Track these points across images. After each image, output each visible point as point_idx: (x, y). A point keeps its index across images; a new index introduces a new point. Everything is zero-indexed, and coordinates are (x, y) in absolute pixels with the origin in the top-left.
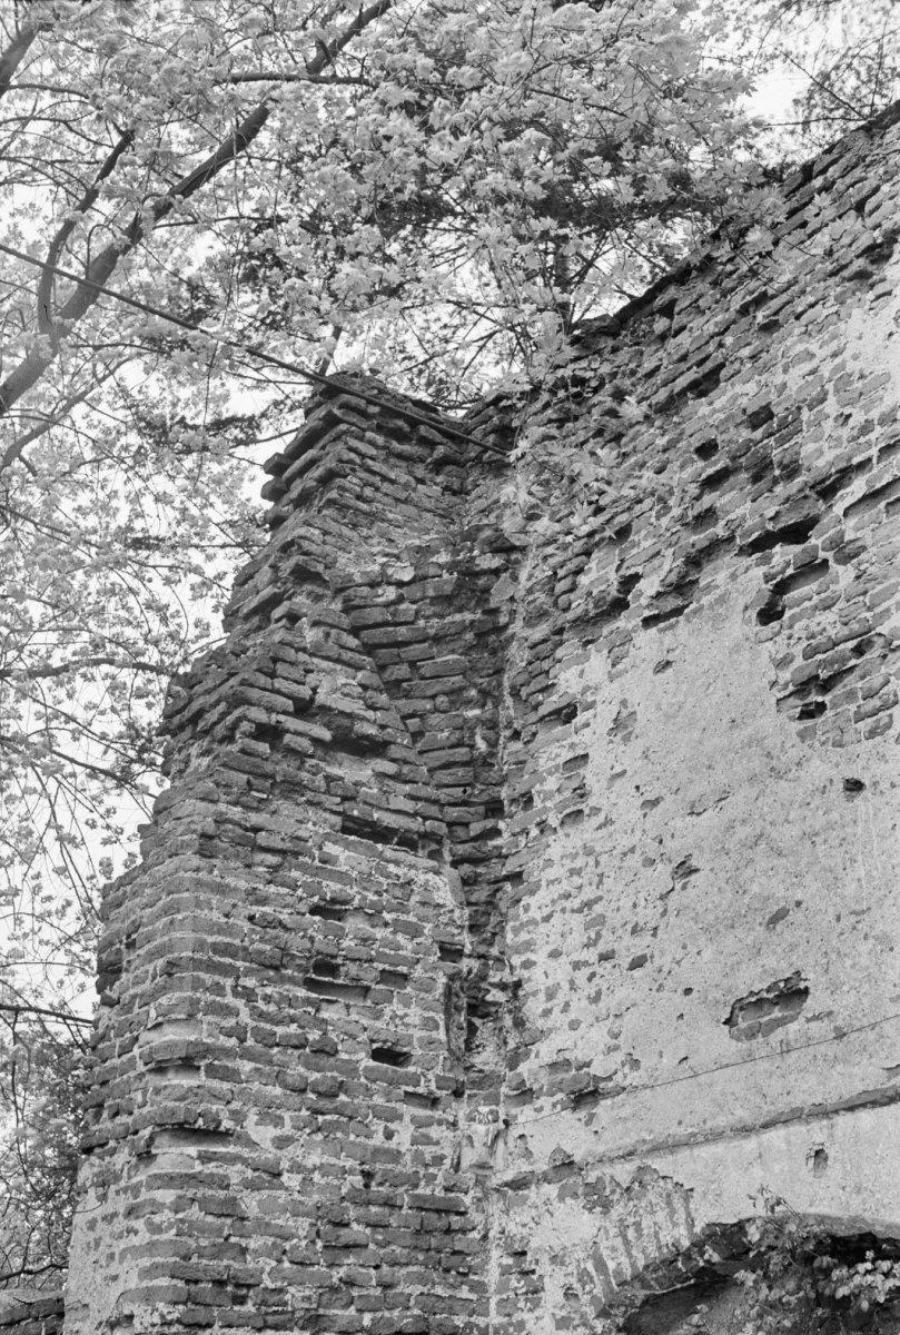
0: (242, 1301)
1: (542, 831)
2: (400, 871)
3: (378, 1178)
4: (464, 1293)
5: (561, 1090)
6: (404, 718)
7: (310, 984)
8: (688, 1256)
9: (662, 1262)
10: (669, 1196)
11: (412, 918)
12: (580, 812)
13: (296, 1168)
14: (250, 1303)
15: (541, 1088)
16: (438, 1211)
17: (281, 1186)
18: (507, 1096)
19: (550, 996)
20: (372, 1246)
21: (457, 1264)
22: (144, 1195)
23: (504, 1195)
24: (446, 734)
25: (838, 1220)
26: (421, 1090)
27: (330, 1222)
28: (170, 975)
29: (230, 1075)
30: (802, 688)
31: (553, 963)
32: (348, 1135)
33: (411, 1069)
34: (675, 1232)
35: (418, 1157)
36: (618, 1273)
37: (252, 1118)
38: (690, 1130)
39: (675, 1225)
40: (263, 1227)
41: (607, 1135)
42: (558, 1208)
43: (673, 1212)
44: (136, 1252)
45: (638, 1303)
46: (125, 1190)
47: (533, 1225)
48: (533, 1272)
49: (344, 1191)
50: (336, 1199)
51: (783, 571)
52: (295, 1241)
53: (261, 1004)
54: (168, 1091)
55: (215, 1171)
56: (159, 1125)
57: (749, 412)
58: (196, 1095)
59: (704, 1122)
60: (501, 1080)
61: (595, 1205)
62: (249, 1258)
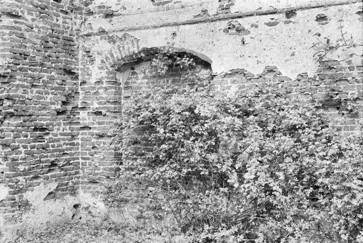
0: (25, 59)
3: (55, 31)
4: (74, 60)
5: (102, 13)
8: (136, 55)
9: (130, 56)
10: (133, 41)
13: (37, 27)
15: (96, 12)
17: (33, 31)
18: (84, 13)
20: (54, 48)
21: (71, 53)
23: (84, 38)
26: (64, 9)
27: (45, 41)
32: (48, 19)
33: (62, 4)
34: (134, 49)
35: (64, 27)
36: (117, 57)
37: (26, 13)
38: (140, 26)
40: (30, 41)
41: (115, 25)
42: (100, 41)
43: (133, 45)
47: (92, 45)
48: (92, 56)
49: (48, 34)
50: (46, 36)
52: (37, 45)
54: (5, 3)
55: (18, 26)
56: (3, 12)
58: (13, 5)
59: (144, 24)
60: (83, 9)
62: (27, 48)
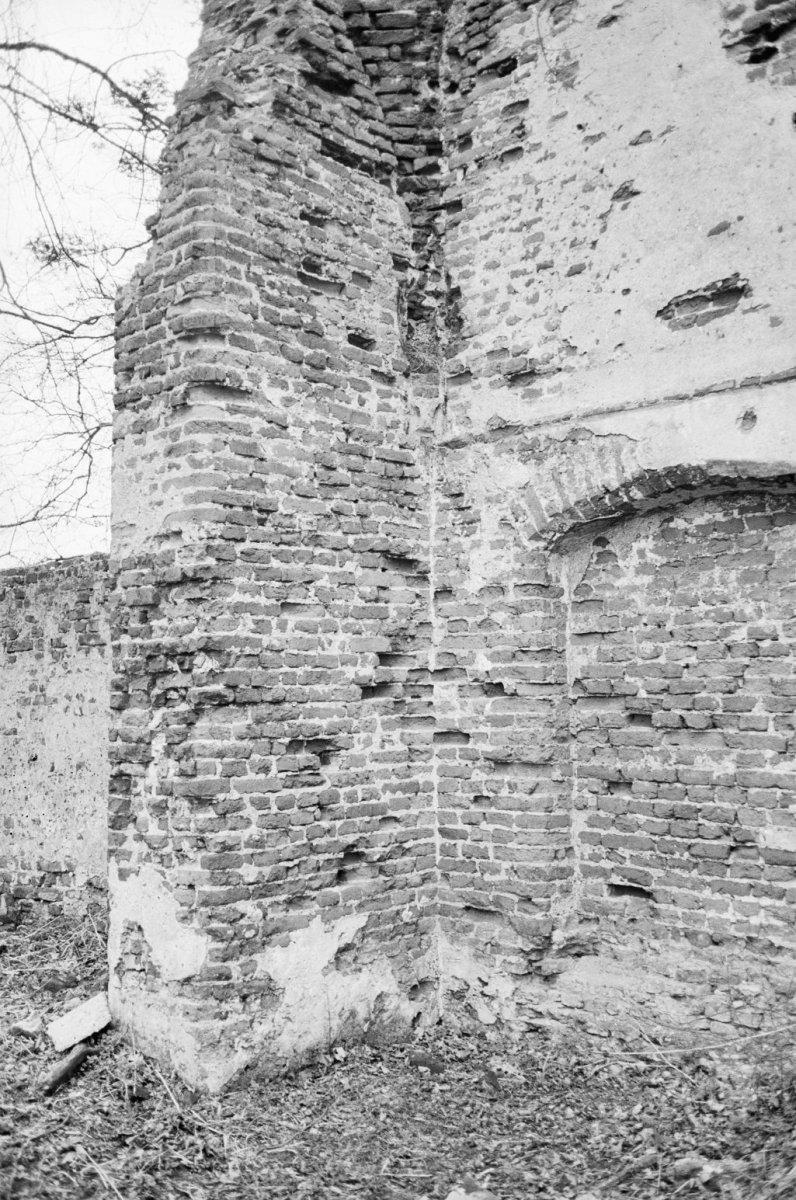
0: (262, 522)
1: (480, 167)
2: (366, 192)
4: (413, 523)
6: (366, 62)
7: (301, 276)
8: (615, 493)
11: (371, 231)
13: (299, 423)
14: (268, 524)
16: (395, 462)
19: (488, 298)
22: (183, 439)
24: (398, 80)
26: (383, 369)
28: (196, 257)
29: (245, 344)
31: (490, 274)
34: (606, 476)
36: (549, 508)
39: (606, 471)
40: (278, 468)
44: (181, 482)
45: (566, 529)
46: (163, 435)
53: (267, 289)
55: (240, 421)
62: (268, 491)
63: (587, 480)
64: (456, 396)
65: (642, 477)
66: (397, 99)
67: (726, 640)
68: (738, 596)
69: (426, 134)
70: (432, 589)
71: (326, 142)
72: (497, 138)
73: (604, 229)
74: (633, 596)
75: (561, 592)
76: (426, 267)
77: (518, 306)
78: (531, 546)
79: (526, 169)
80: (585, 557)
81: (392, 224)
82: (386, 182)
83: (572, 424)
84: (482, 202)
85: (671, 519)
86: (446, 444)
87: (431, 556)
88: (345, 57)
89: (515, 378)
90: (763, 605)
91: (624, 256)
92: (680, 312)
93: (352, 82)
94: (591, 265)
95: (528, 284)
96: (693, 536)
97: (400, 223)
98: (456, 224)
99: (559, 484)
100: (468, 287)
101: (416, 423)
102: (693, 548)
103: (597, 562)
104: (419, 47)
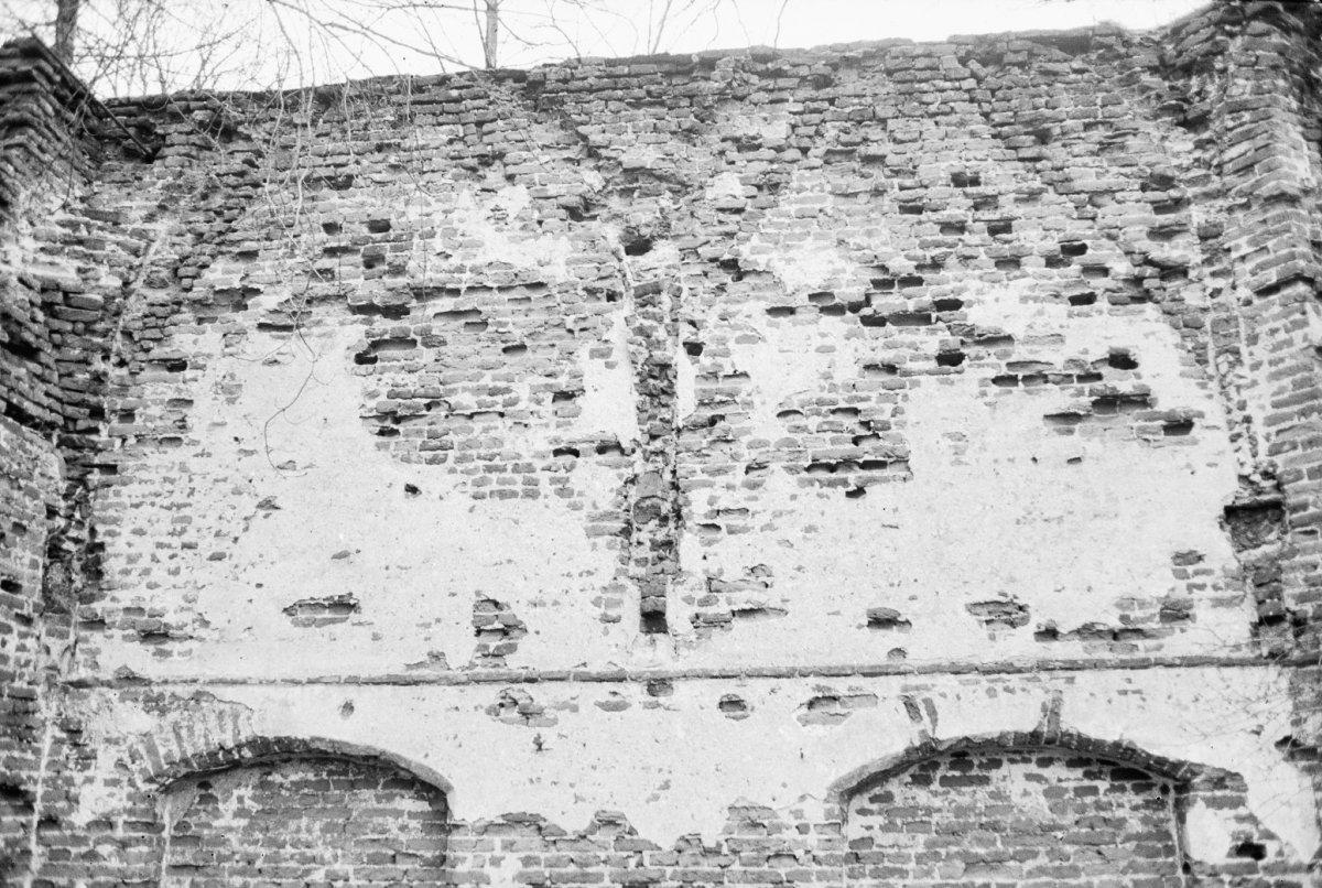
2: (34, 449)
6: (52, 332)
8: (229, 752)
11: (33, 485)
12: (179, 439)
24: (77, 352)
25: (357, 746)
26: (25, 612)
30: (383, 416)
31: (136, 539)
34: (223, 736)
36: (168, 755)
51: (381, 335)
57: (371, 218)
61: (152, 709)
63: (206, 736)
64: (86, 640)
65: (255, 741)
66: (73, 367)
67: (307, 879)
68: (320, 843)
69: (93, 400)
70: (35, 818)
71: (10, 404)
72: (159, 423)
73: (246, 529)
74: (228, 836)
75: (163, 827)
76: (72, 516)
77: (158, 574)
78: (144, 787)
79: (183, 459)
80: (189, 797)
81: (51, 478)
82: (48, 437)
83: (196, 687)
84: (137, 474)
85: (269, 774)
86: (71, 684)
87: (39, 785)
88: (36, 327)
89: (148, 636)
90: (340, 852)
91: (261, 556)
92: (303, 612)
93: (39, 350)
94: (231, 556)
95: (172, 557)
96: (288, 789)
97: (58, 476)
98: (109, 486)
99: (178, 736)
100: (112, 545)
101: (43, 661)
102: (286, 800)
103: (200, 803)
104: (100, 326)
